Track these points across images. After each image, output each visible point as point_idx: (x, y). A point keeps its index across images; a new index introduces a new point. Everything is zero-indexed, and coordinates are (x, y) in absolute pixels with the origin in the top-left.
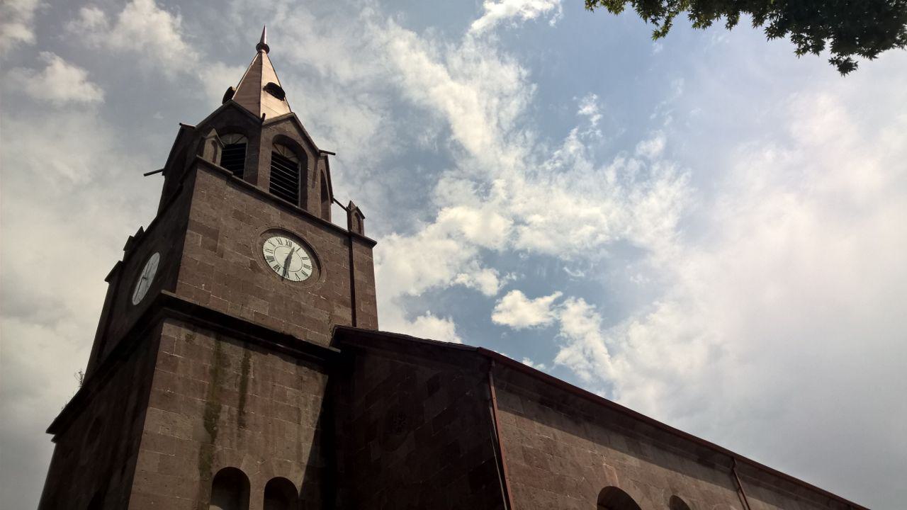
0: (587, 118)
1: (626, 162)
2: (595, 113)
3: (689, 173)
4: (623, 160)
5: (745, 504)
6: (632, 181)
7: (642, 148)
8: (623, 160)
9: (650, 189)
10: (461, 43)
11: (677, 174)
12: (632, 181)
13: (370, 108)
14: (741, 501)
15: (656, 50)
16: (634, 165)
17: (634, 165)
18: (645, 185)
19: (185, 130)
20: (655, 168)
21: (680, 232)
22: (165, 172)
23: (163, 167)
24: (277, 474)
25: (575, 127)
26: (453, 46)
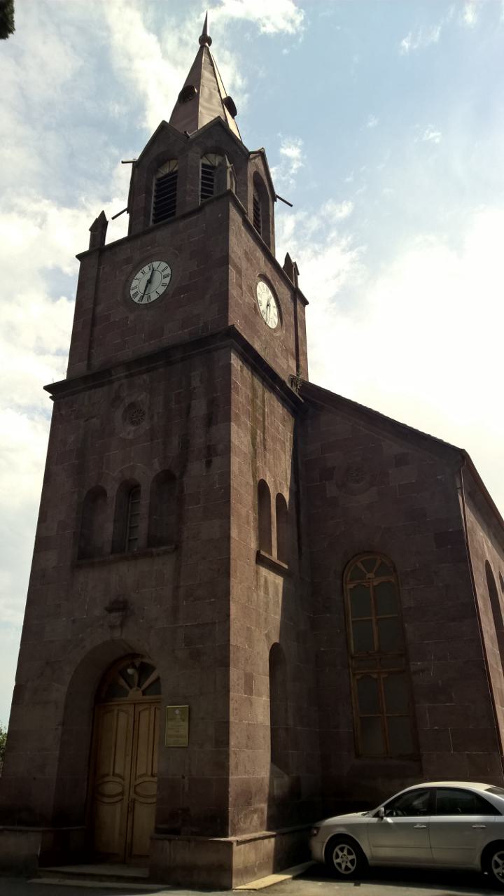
0: (289, 160)
1: (309, 217)
2: (298, 160)
3: (364, 248)
4: (305, 214)
5: (151, 746)
6: (307, 238)
7: (329, 207)
8: (305, 214)
9: (320, 254)
10: (183, 20)
11: (351, 248)
12: (307, 238)
13: (73, 47)
14: (149, 730)
15: (370, 124)
16: (314, 224)
17: (314, 224)
18: (317, 247)
19: (305, 302)
20: (334, 234)
21: (334, 305)
22: (128, 210)
23: (126, 206)
24: (280, 492)
25: (275, 166)
26: (173, 21)
